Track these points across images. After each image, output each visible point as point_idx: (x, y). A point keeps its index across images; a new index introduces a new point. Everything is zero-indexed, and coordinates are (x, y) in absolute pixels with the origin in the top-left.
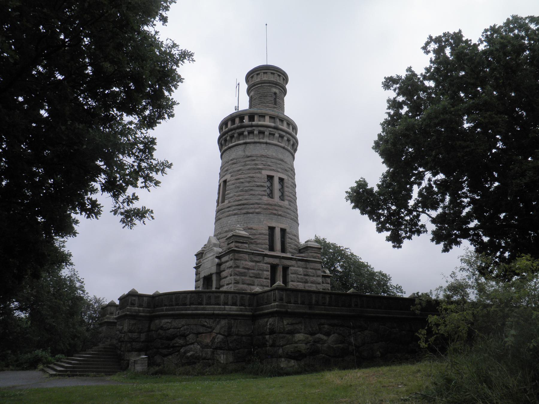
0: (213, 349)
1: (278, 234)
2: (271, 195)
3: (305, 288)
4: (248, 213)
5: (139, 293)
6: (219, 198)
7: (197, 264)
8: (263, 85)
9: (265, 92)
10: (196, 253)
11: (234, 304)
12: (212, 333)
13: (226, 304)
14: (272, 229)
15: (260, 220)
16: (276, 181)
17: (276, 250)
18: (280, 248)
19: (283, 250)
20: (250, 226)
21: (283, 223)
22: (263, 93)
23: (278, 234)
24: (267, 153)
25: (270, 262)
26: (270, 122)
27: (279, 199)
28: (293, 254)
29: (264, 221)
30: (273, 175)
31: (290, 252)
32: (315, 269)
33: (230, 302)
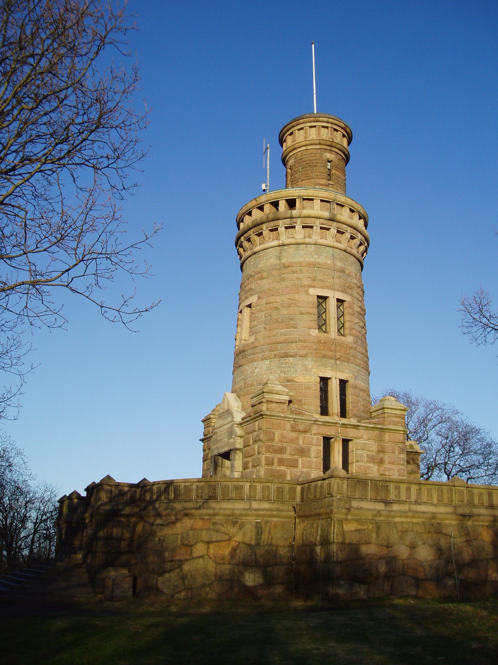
0: (233, 565)
1: (334, 388)
2: (322, 326)
3: (315, 321)
4: (286, 355)
5: (136, 483)
6: (334, 459)
7: (205, 435)
8: (308, 148)
9: (312, 160)
10: (203, 418)
11: (266, 499)
12: (230, 542)
13: (251, 499)
14: (324, 381)
15: (307, 367)
16: (332, 304)
17: (333, 414)
18: (339, 411)
19: (343, 414)
20: (289, 376)
21: (343, 372)
22: (310, 160)
23: (334, 388)
24: (318, 260)
25: (322, 433)
26: (321, 210)
27: (337, 334)
28: (360, 418)
29: (312, 368)
30: (327, 296)
31: (355, 416)
32: (331, 150)
33: (259, 495)
